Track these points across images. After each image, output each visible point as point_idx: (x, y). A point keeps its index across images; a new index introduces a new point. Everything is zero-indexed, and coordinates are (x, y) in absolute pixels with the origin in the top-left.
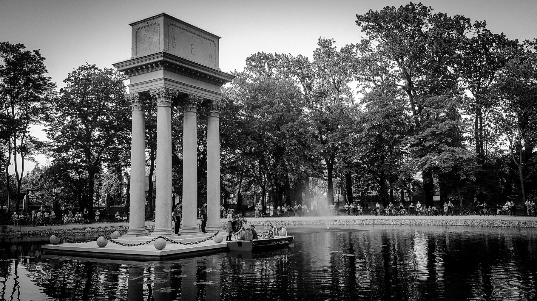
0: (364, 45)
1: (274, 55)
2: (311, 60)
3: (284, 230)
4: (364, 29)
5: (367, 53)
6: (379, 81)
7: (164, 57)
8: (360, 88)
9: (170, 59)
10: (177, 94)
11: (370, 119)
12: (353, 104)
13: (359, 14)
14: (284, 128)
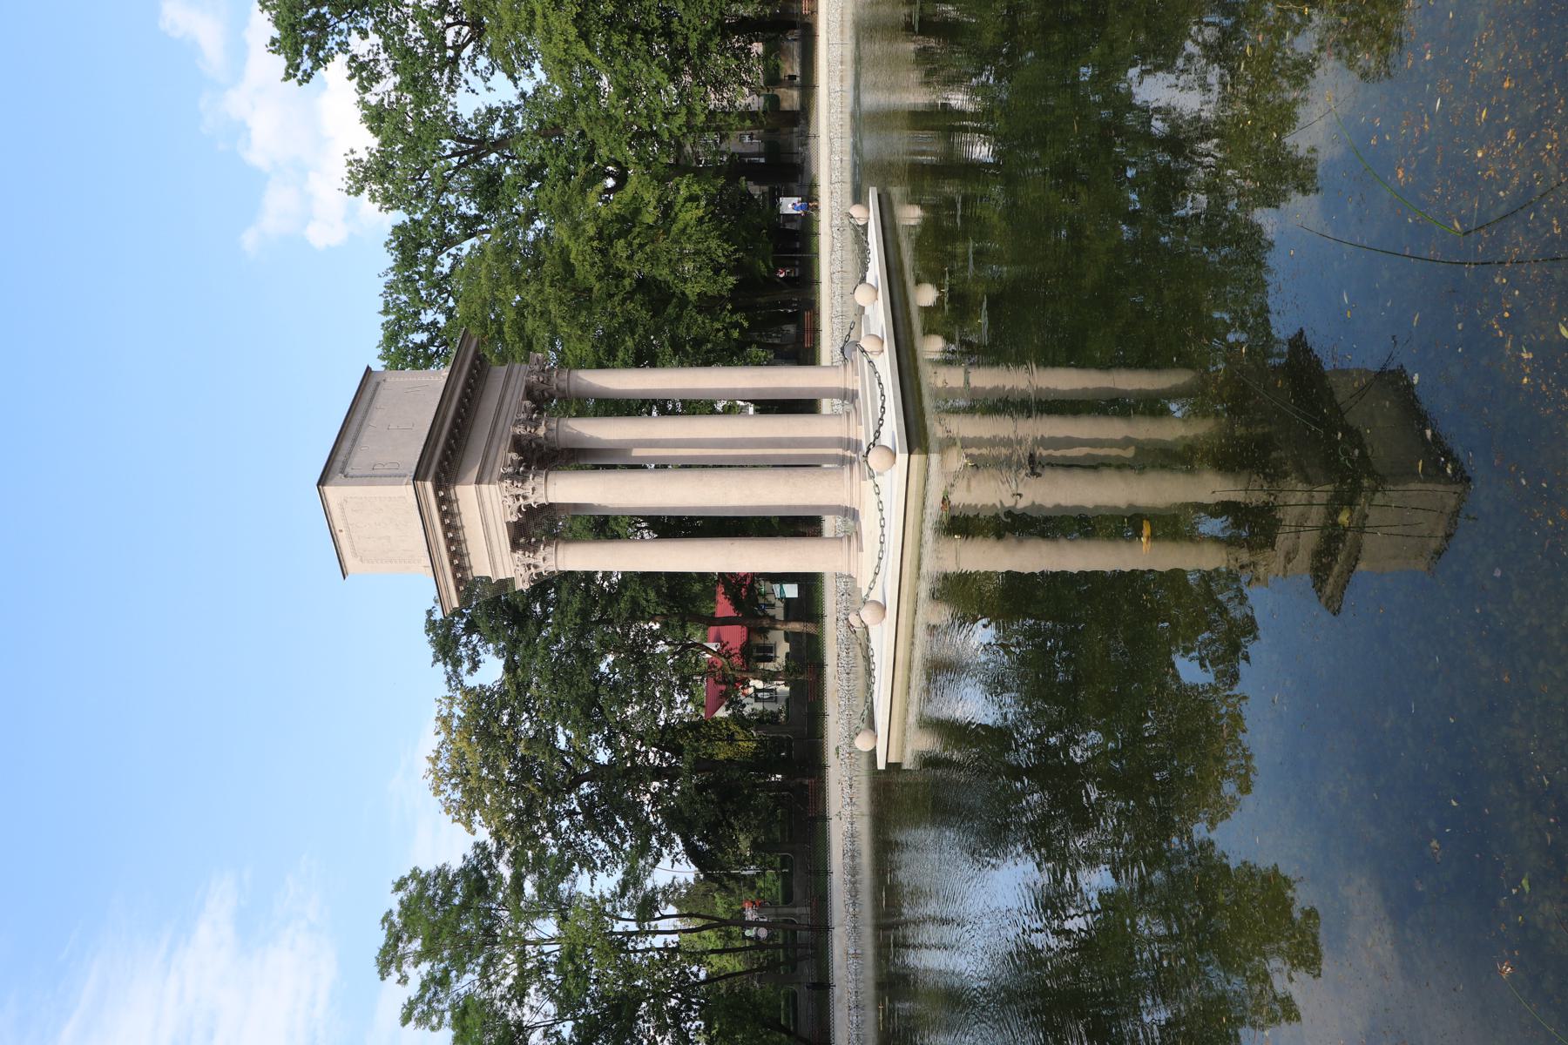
0: (364, 73)
1: (384, 319)
2: (399, 217)
3: (857, 211)
4: (319, 63)
5: (383, 64)
6: (458, 33)
7: (424, 479)
8: (476, 83)
9: (450, 400)
10: (528, 403)
11: (562, 45)
12: (518, 107)
13: (283, 75)
14: (586, 272)
